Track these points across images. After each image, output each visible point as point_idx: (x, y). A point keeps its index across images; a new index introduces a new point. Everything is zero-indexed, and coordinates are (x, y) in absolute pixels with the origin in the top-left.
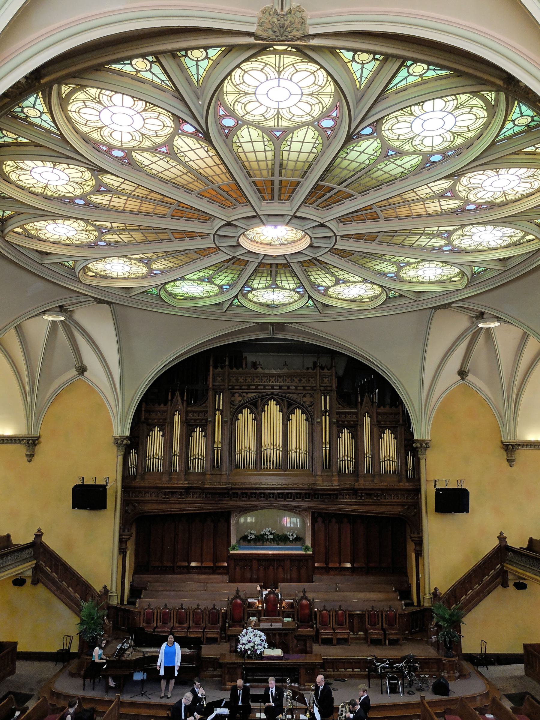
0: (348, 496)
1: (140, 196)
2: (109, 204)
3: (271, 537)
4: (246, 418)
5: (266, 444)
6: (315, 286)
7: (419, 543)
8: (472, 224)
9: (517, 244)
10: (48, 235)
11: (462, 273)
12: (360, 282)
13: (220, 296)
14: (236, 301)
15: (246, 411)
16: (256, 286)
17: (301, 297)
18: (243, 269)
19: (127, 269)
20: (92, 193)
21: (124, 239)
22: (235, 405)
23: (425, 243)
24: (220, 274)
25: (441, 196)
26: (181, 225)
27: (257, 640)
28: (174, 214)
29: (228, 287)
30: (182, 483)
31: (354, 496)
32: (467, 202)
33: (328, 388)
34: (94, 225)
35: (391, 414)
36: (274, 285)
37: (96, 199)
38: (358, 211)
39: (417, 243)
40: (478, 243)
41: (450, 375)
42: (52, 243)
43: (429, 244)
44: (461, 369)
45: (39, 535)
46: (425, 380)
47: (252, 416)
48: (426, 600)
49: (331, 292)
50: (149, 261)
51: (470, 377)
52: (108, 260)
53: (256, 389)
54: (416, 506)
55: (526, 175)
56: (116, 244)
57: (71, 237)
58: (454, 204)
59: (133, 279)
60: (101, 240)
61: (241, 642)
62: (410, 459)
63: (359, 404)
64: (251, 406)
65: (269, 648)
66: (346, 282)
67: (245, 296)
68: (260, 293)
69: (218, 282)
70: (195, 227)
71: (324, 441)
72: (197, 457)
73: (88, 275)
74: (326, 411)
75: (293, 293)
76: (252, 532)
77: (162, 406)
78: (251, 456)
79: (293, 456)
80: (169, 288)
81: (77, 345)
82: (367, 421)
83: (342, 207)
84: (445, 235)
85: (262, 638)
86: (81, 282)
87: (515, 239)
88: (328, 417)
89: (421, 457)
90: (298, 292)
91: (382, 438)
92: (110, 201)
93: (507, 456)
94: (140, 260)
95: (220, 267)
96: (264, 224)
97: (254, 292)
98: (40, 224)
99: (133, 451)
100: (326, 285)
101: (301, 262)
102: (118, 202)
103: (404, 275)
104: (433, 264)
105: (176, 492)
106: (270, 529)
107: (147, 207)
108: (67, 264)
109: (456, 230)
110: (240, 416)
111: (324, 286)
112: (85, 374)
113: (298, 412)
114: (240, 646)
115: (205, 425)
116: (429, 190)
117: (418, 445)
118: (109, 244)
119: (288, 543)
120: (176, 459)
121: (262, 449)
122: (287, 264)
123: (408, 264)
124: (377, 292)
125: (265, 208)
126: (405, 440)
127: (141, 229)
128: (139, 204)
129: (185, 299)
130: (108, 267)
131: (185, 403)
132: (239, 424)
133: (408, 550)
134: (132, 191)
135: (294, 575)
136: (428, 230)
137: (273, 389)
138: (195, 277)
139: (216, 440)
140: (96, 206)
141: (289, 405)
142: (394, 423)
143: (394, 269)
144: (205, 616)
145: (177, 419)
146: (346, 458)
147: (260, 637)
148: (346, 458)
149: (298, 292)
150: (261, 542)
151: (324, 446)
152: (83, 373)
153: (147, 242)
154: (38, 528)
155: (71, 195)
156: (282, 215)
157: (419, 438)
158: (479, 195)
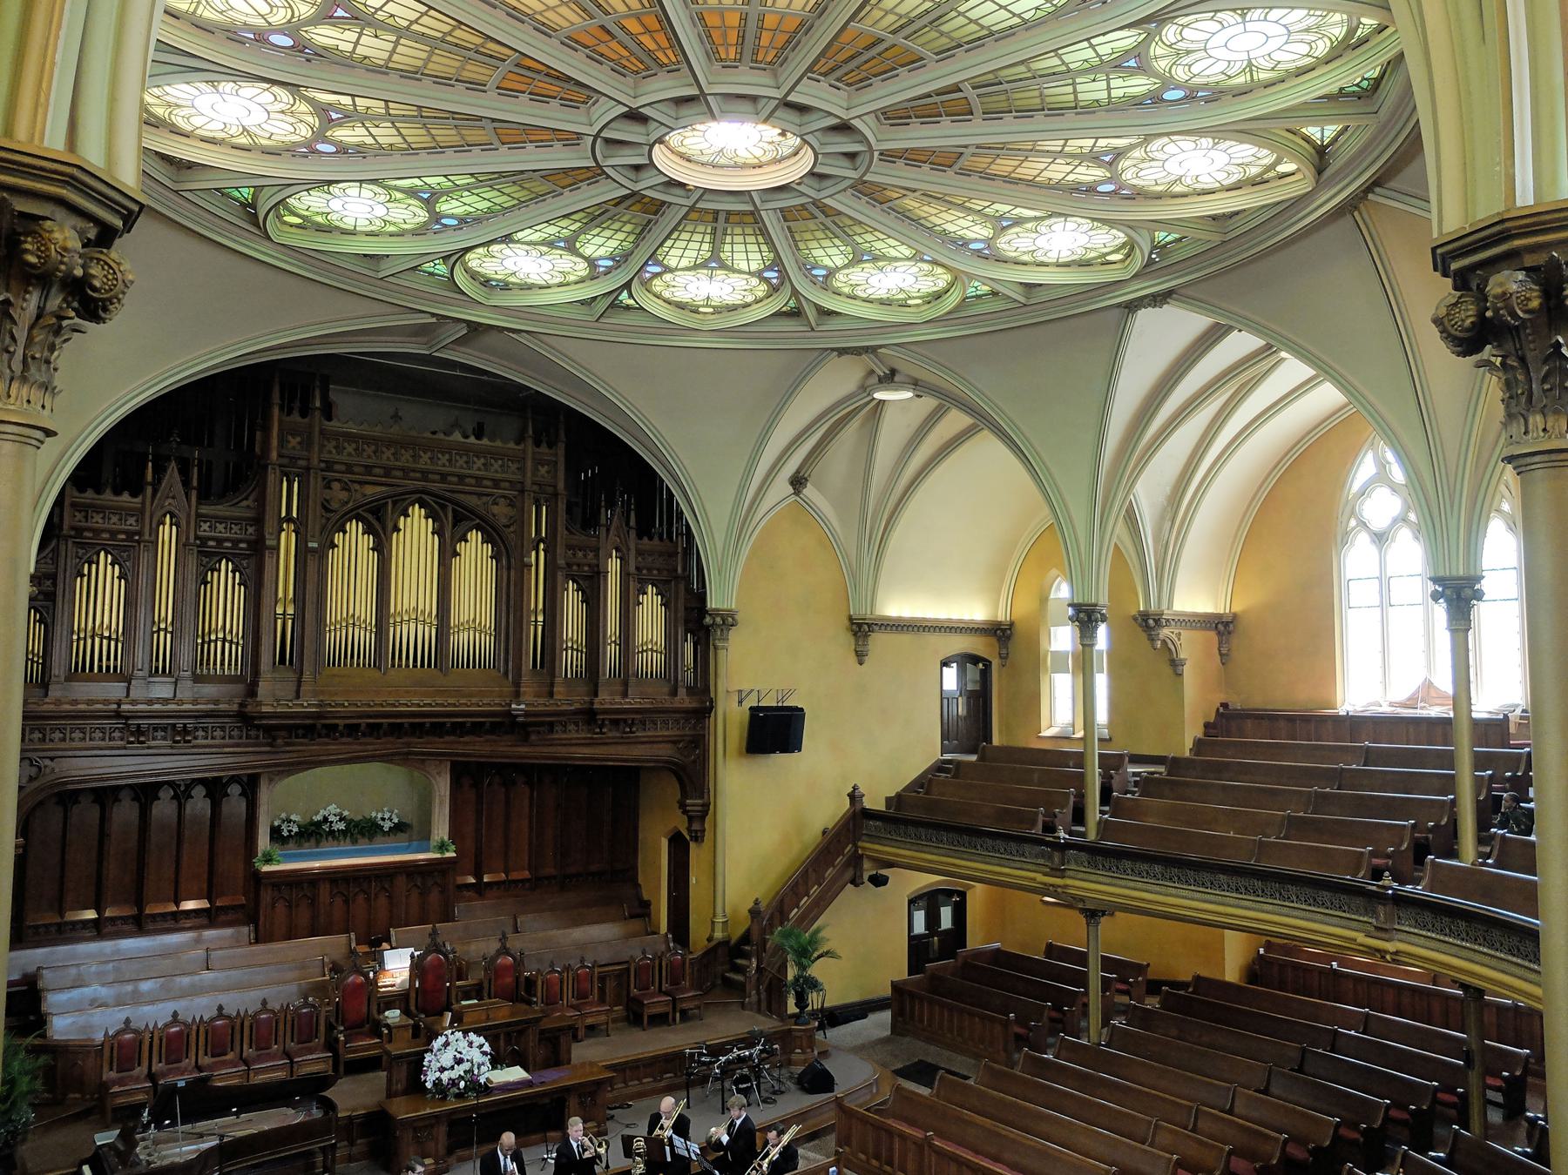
1: (429, 37)
2: (354, 51)
3: (342, 826)
4: (354, 543)
6: (807, 268)
8: (1168, 134)
9: (1257, 182)
10: (197, 121)
11: (1130, 247)
12: (908, 259)
13: (588, 283)
14: (625, 294)
15: (354, 528)
16: (673, 263)
17: (774, 290)
18: (649, 221)
19: (380, 211)
20: (314, 21)
21: (380, 140)
23: (1060, 176)
24: (595, 232)
25: (1116, 65)
26: (521, 111)
28: (506, 84)
29: (610, 263)
32: (1168, 82)
34: (311, 101)
36: (715, 262)
37: (324, 36)
38: (929, 95)
39: (1045, 174)
40: (1173, 178)
42: (204, 140)
43: (1071, 177)
49: (840, 281)
50: (433, 194)
51: (809, 491)
52: (334, 189)
55: (1303, 25)
56: (360, 151)
57: (253, 130)
58: (1139, 85)
59: (392, 235)
60: (326, 140)
62: (689, 648)
64: (370, 517)
66: (875, 259)
67: (646, 284)
68: (682, 278)
69: (588, 251)
70: (552, 116)
72: (221, 635)
73: (285, 223)
75: (755, 281)
76: (293, 817)
78: (364, 637)
79: (461, 640)
80: (474, 260)
82: (614, 566)
83: (892, 86)
84: (1107, 159)
86: (269, 238)
87: (1254, 171)
88: (542, 554)
89: (719, 644)
90: (767, 280)
92: (357, 43)
93: (857, 644)
94: (412, 193)
95: (596, 218)
96: (713, 117)
97: (667, 277)
98: (179, 91)
100: (830, 264)
101: (782, 210)
102: (374, 47)
103: (1005, 247)
104: (1071, 224)
106: (333, 808)
107: (444, 63)
108: (236, 194)
109: (1132, 147)
110: (338, 538)
111: (825, 267)
113: (475, 537)
115: (253, 561)
116: (1090, 53)
118: (343, 150)
119: (379, 838)
122: (752, 213)
123: (1019, 221)
124: (942, 284)
125: (718, 83)
127: (422, 116)
128: (424, 55)
129: (718, 310)
130: (336, 204)
131: (194, 494)
132: (336, 558)
133: (640, 836)
134: (412, 23)
135: (303, 917)
136: (1074, 145)
138: (536, 237)
140: (323, 55)
141: (458, 519)
143: (987, 232)
144: (281, 1026)
145: (167, 534)
149: (767, 280)
150: (313, 841)
153: (436, 149)
155: (261, 22)
156: (754, 99)
158: (1195, 69)
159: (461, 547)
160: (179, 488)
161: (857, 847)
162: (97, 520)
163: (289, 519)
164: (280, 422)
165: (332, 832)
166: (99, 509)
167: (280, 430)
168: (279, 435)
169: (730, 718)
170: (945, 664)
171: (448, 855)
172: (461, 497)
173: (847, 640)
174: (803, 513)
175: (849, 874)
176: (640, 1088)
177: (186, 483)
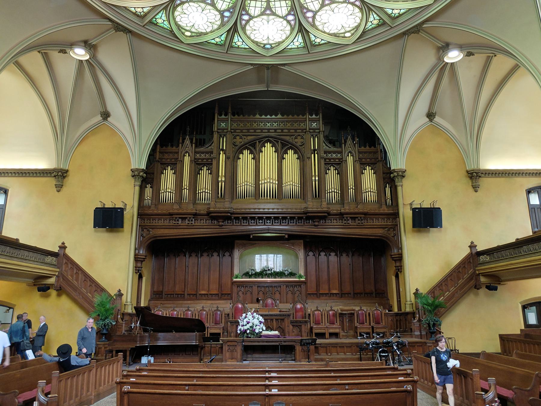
0: (335, 221)
4: (246, 158)
5: (263, 178)
7: (400, 258)
15: (246, 152)
22: (236, 146)
27: (256, 322)
30: (190, 209)
31: (340, 221)
33: (317, 131)
35: (370, 153)
41: (419, 119)
44: (429, 111)
45: (63, 247)
46: (400, 120)
47: (251, 156)
48: (408, 306)
51: (437, 119)
53: (255, 132)
54: (395, 227)
61: (241, 324)
62: (388, 190)
63: (343, 145)
64: (251, 147)
65: (267, 330)
71: (313, 174)
74: (314, 150)
77: (174, 148)
81: (99, 83)
82: (350, 160)
85: (260, 320)
88: (316, 155)
91: (363, 174)
93: (472, 183)
99: (149, 186)
105: (186, 218)
112: (109, 119)
114: (239, 327)
115: (209, 163)
117: (395, 174)
120: (186, 192)
121: (260, 183)
126: (383, 173)
131: (194, 145)
132: (240, 162)
133: (388, 278)
137: (269, 132)
139: (220, 174)
141: (283, 145)
142: (373, 160)
144: (209, 316)
145: (187, 159)
146: (333, 190)
147: (258, 319)
148: (333, 190)
151: (313, 178)
152: (107, 118)
154: (60, 244)
157: (395, 168)
159: (285, 156)
160: (189, 145)
161: (475, 270)
162: (166, 156)
163: (222, 150)
164: (218, 118)
165: (266, 274)
166: (166, 153)
167: (218, 121)
168: (221, 123)
169: (406, 215)
170: (529, 192)
171: (302, 279)
172: (281, 137)
173: (467, 183)
174: (438, 130)
175: (472, 282)
176: (344, 357)
177: (192, 142)
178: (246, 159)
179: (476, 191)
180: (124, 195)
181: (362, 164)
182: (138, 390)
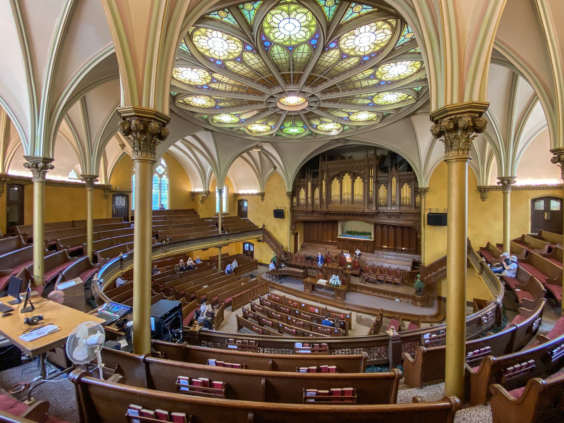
15: (335, 179)
32: (381, 81)
47: (338, 181)
58: (375, 82)
87: (403, 99)
120: (309, 200)
123: (353, 113)
132: (333, 185)
145: (309, 184)
168: (323, 165)
169: (425, 213)
178: (336, 183)
179: (483, 201)
180: (285, 204)
181: (400, 184)
182: (18, 131)
